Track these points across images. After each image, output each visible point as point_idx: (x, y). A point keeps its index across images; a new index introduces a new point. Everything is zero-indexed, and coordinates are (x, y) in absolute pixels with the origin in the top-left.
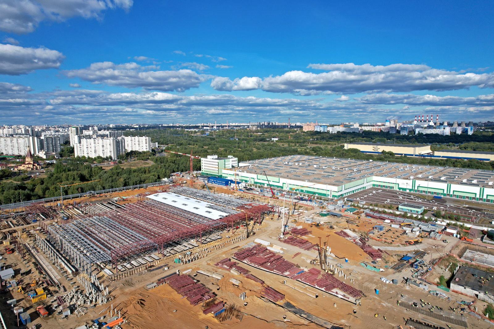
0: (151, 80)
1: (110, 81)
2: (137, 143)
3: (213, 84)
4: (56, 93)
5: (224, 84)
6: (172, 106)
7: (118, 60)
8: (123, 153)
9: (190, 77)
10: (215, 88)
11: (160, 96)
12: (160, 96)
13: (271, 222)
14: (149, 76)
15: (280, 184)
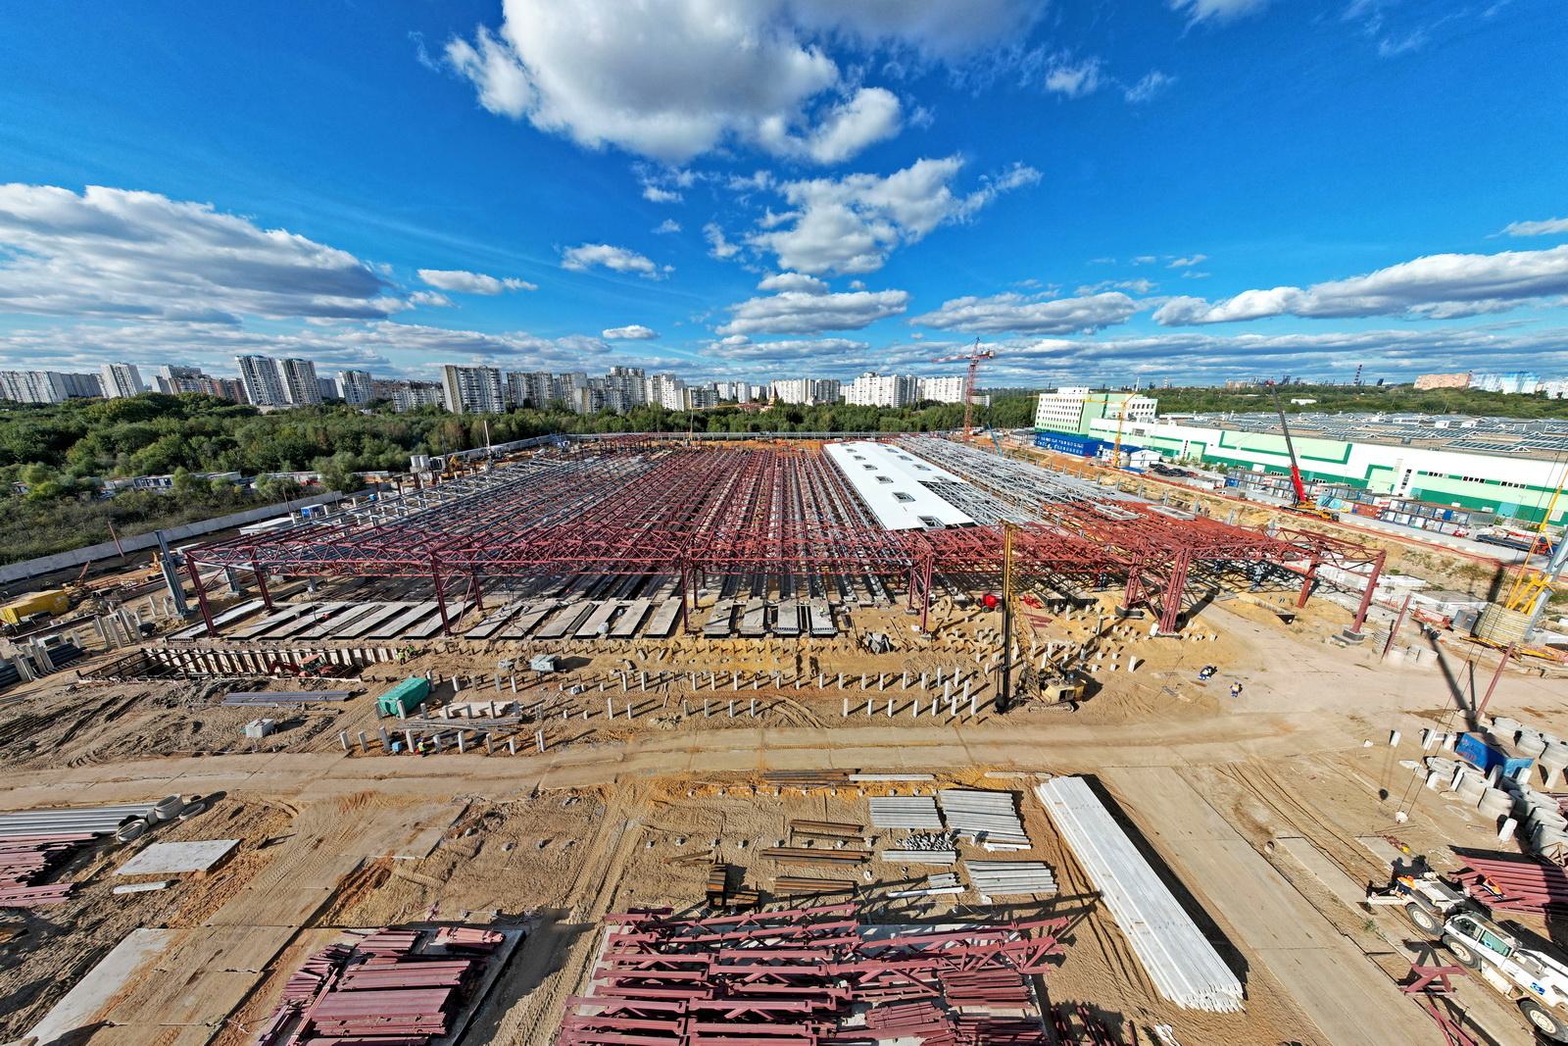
0: (1039, 317)
1: (964, 326)
2: (943, 388)
3: (1162, 312)
4: (894, 349)
5: (1188, 310)
6: (1063, 361)
7: (984, 292)
8: (912, 399)
9: (1113, 306)
10: (1163, 322)
11: (1049, 344)
12: (1049, 344)
13: (1270, 640)
14: (1034, 312)
15: (1355, 470)
